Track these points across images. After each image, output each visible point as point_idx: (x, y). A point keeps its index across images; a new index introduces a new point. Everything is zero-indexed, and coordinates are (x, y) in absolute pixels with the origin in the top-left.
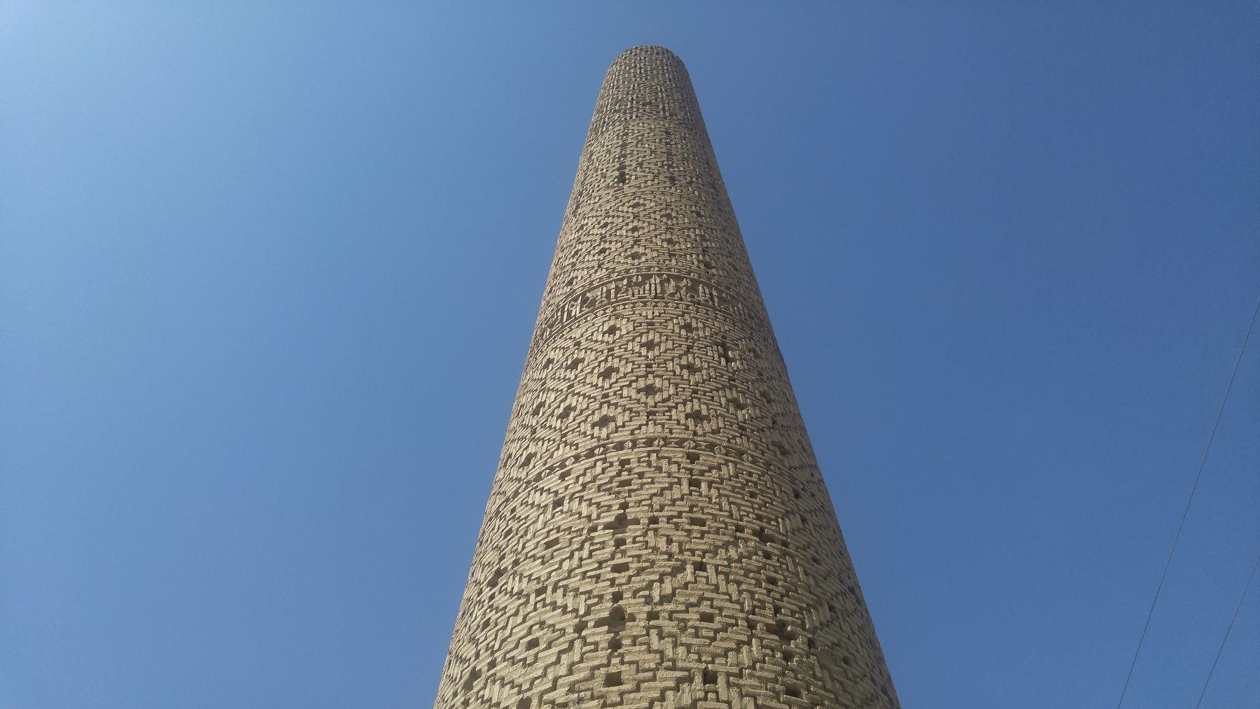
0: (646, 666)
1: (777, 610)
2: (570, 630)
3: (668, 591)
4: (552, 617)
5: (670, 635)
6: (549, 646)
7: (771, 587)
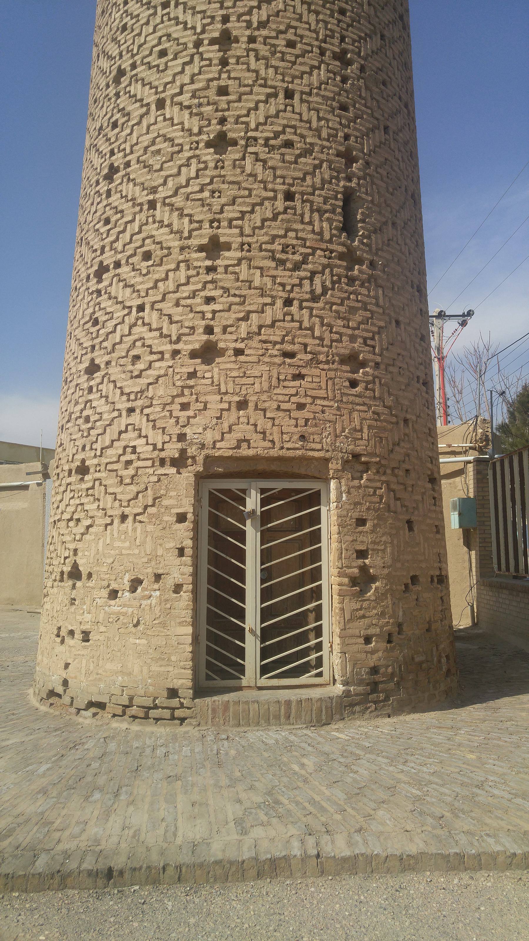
0: (246, 82)
1: (343, 39)
2: (190, 45)
3: (264, 18)
4: (176, 31)
5: (265, 58)
6: (175, 58)
7: (341, 17)
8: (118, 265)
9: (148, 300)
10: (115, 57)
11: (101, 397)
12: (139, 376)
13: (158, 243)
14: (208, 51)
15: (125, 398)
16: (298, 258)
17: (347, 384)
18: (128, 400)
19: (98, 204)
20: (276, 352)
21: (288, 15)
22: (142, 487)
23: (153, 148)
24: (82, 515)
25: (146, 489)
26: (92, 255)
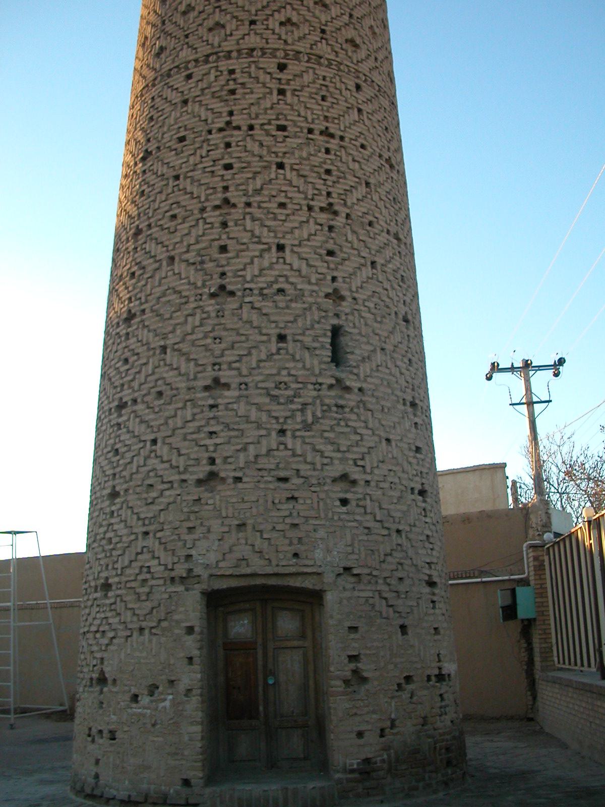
2: (196, 212)
3: (258, 187)
4: (184, 199)
8: (135, 401)
9: (160, 435)
10: (134, 217)
11: (121, 521)
12: (152, 503)
13: (168, 384)
14: (210, 217)
15: (140, 523)
16: (290, 393)
17: (338, 503)
18: (144, 525)
19: (118, 344)
20: (270, 479)
21: (279, 182)
22: (155, 604)
23: (163, 299)
24: (107, 628)
25: (159, 605)
26: (113, 391)
